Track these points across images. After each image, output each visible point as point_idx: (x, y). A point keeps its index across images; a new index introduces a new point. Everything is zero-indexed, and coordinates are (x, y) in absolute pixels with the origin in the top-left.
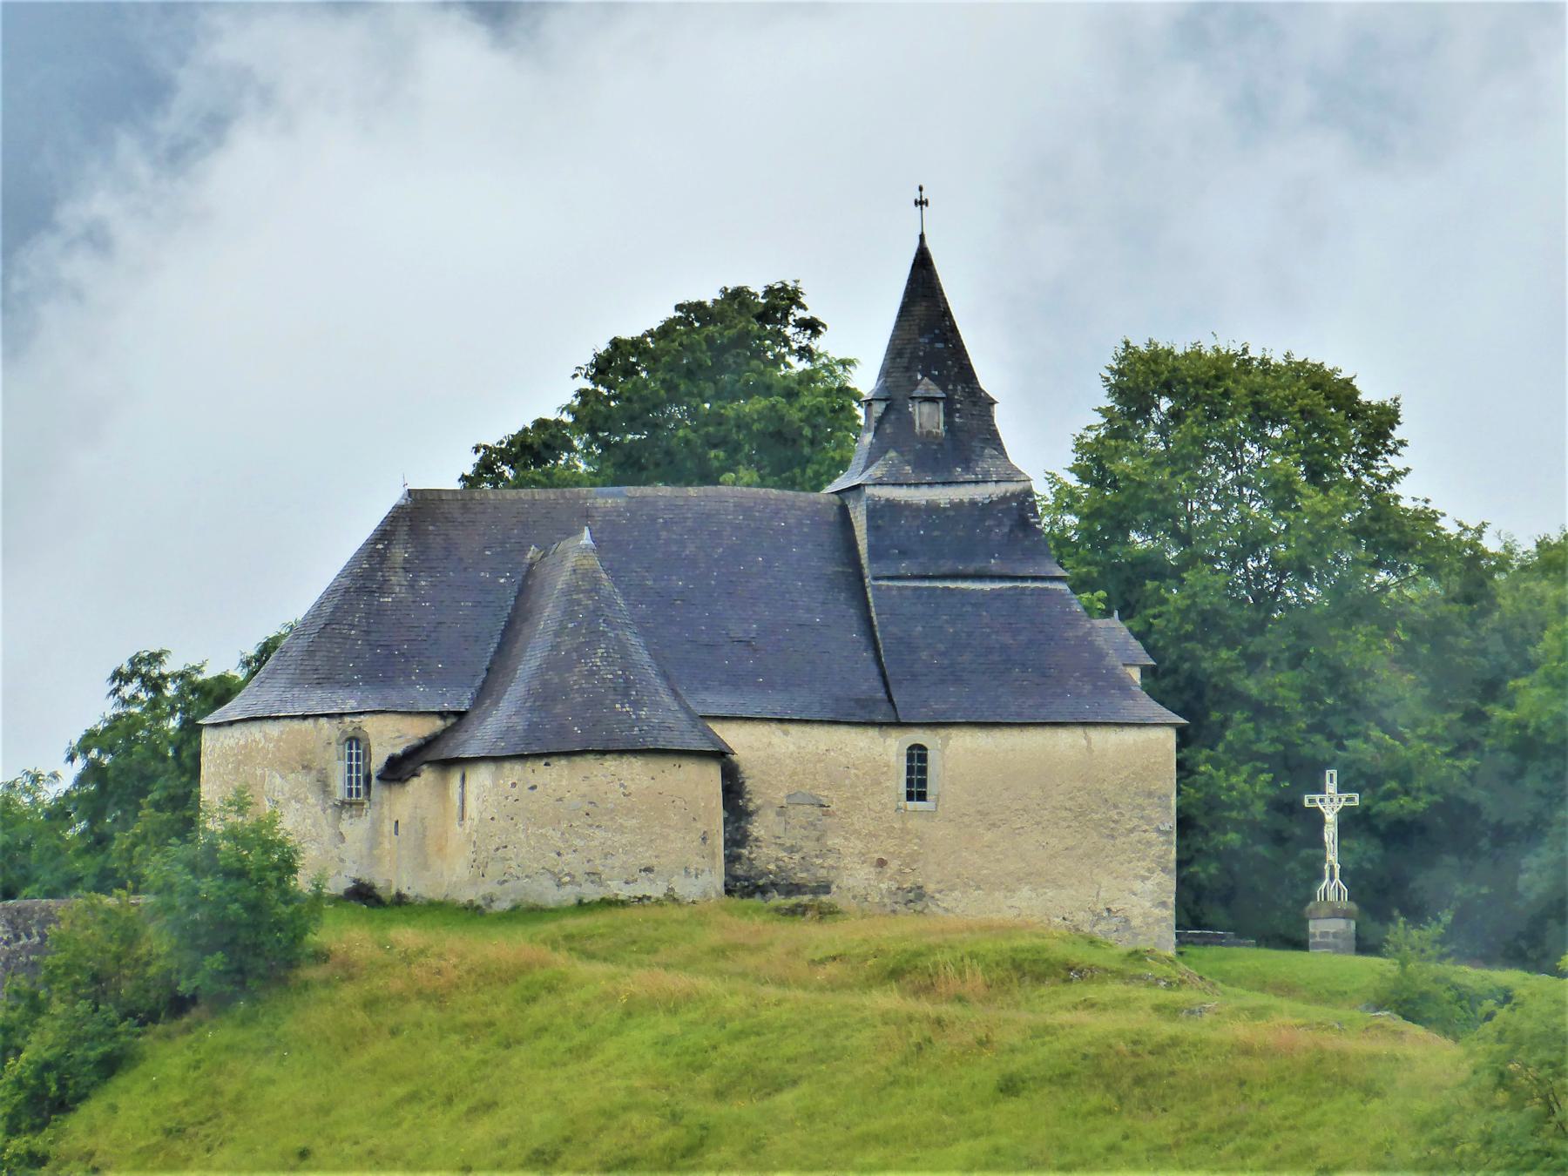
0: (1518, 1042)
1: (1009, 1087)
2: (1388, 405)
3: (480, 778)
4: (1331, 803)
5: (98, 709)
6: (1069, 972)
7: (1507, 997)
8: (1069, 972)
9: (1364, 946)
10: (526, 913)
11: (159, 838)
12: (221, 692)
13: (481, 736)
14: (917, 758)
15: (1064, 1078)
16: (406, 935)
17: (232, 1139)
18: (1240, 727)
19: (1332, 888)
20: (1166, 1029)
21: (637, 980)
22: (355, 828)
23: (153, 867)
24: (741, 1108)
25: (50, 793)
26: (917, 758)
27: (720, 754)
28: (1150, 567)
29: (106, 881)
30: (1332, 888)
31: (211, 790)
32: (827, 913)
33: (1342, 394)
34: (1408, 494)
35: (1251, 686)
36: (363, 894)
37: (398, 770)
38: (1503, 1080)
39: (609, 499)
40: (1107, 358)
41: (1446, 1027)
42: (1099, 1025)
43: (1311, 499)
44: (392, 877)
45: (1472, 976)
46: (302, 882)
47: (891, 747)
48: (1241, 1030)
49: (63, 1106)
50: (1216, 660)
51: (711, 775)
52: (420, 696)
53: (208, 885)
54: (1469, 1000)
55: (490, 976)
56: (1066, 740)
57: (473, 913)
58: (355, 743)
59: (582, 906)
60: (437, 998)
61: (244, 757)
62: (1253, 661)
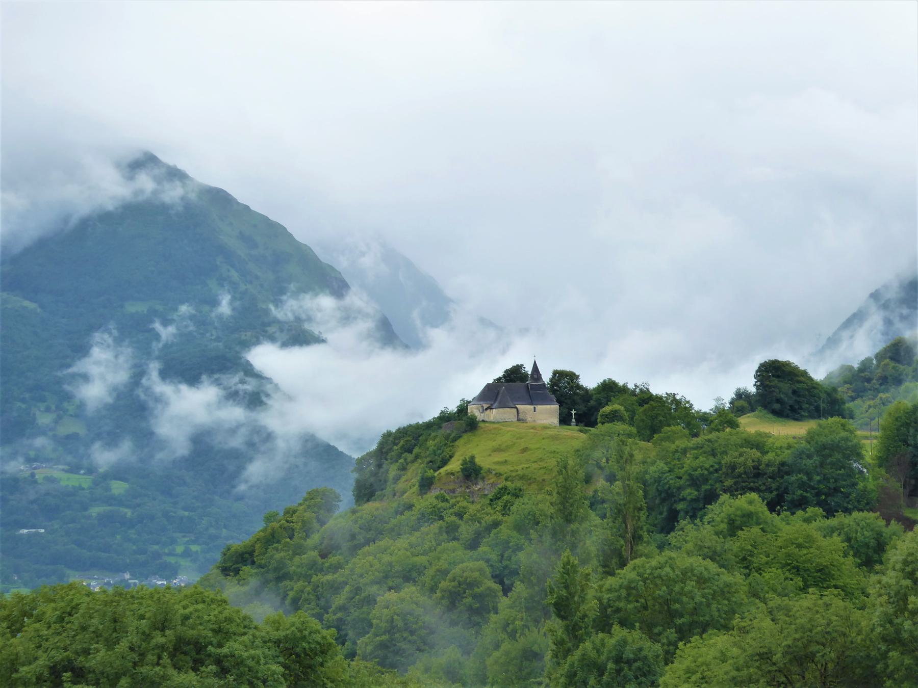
0: (591, 435)
1: (543, 439)
2: (482, 471)
3: (494, 410)
4: (573, 412)
5: (459, 404)
6: (549, 428)
7: (590, 430)
8: (549, 428)
9: (577, 425)
10: (498, 422)
11: (464, 416)
12: (470, 402)
13: (494, 406)
14: (535, 408)
15: (548, 438)
16: (487, 425)
17: (500, 433)
18: (564, 405)
19: (574, 420)
20: (558, 433)
21: (509, 429)
22: (482, 415)
23: (464, 418)
24: (518, 441)
25: (454, 411)
26: (535, 408)
27: (516, 408)
28: (556, 390)
29: (459, 420)
30: (574, 420)
31: (469, 411)
32: (526, 423)
33: (574, 374)
34: (580, 383)
35: (566, 401)
36: (483, 421)
37: (486, 409)
38: (590, 438)
39: (506, 384)
40: (552, 371)
41: (585, 433)
42: (552, 433)
43: (571, 384)
44: (486, 419)
45: (587, 428)
46: (478, 420)
47: (532, 407)
48: (565, 433)
49: (456, 441)
50: (563, 399)
51: (516, 410)
52: (488, 402)
53: (469, 420)
54: (586, 430)
55: (495, 428)
56: (548, 406)
57: (494, 423)
58: (482, 407)
59: (503, 422)
60: (490, 431)
61: (472, 408)
62: (566, 399)
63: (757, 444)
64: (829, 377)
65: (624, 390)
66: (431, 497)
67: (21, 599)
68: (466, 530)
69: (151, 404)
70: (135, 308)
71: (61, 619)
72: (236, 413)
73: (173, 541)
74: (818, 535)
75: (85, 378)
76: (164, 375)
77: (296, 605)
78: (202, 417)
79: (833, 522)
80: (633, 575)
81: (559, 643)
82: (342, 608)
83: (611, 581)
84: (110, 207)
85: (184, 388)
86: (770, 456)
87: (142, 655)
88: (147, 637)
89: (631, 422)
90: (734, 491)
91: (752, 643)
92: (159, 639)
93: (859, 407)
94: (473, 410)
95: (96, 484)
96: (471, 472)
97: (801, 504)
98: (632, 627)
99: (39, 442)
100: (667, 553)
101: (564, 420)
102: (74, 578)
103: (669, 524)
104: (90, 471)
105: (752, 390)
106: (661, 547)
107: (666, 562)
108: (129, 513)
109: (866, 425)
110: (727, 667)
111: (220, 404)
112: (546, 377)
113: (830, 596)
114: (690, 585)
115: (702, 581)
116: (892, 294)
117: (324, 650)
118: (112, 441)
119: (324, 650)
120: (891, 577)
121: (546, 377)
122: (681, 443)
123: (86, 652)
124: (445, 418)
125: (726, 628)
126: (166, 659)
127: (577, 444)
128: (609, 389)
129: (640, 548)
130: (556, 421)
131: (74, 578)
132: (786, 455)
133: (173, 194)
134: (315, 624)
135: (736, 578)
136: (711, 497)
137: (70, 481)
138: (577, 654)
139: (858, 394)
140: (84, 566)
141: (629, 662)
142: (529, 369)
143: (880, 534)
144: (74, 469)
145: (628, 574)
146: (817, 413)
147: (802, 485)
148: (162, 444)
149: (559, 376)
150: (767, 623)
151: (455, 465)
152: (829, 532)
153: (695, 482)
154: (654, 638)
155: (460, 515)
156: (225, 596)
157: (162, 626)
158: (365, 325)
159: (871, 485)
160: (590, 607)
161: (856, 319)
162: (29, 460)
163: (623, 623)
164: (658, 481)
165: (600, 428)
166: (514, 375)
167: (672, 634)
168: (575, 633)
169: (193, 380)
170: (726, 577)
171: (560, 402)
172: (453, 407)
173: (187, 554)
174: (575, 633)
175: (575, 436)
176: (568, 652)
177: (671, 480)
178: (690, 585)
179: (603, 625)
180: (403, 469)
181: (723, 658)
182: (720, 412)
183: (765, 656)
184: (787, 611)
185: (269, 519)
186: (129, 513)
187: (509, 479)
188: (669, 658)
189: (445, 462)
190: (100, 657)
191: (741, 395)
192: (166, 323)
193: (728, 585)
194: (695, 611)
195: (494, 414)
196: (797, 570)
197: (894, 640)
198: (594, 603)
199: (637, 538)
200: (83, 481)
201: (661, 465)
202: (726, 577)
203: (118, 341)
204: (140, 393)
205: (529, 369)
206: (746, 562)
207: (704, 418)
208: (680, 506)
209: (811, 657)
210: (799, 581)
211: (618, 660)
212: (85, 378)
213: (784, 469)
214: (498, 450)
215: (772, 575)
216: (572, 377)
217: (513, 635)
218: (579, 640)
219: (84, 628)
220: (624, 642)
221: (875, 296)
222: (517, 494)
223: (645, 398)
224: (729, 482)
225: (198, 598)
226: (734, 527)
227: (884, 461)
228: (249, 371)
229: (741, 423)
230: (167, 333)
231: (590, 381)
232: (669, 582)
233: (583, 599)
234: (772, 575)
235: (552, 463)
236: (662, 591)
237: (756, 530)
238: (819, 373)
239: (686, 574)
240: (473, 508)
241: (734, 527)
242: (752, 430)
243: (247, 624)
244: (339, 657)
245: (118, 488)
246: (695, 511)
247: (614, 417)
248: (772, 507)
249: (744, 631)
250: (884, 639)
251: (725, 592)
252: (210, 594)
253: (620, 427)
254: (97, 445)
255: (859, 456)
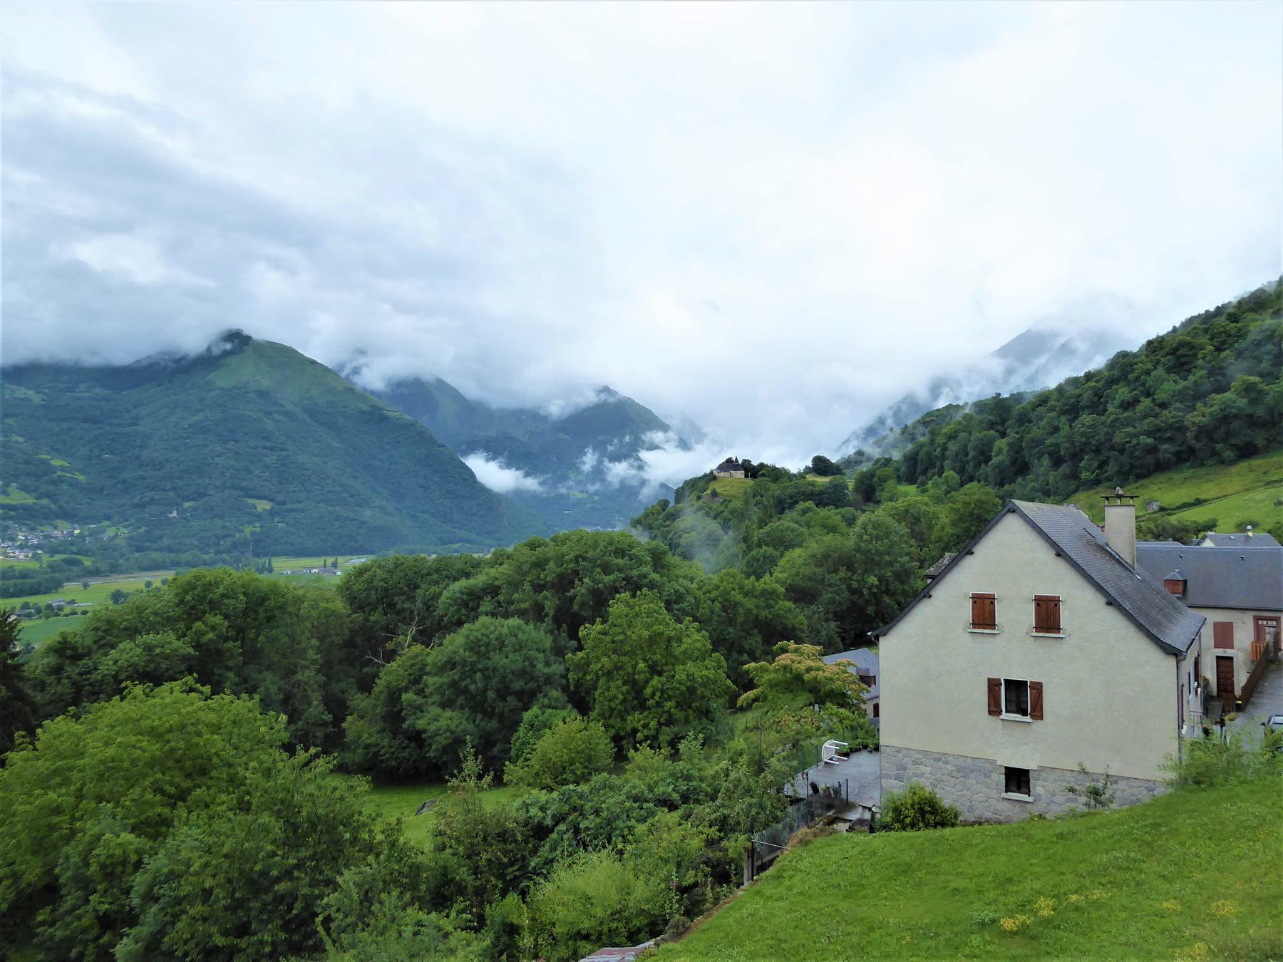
63: (813, 484)
64: (838, 461)
65: (767, 466)
66: (700, 502)
67: (565, 534)
68: (712, 514)
69: (605, 470)
70: (600, 438)
71: (578, 541)
72: (634, 472)
73: (615, 516)
74: (833, 516)
75: (584, 463)
76: (610, 461)
77: (654, 538)
78: (622, 473)
79: (838, 511)
80: (769, 529)
81: (744, 551)
82: (671, 539)
83: (762, 531)
84: (591, 405)
85: (617, 464)
86: (817, 488)
87: (605, 553)
88: (606, 547)
89: (769, 477)
90: (805, 500)
91: (810, 552)
92: (610, 548)
93: (846, 471)
94: (715, 473)
95: (589, 496)
96: (714, 494)
97: (827, 505)
98: (769, 546)
99: (571, 483)
100: (781, 521)
101: (746, 476)
102: (582, 528)
103: (782, 512)
104: (587, 492)
105: (811, 466)
106: (779, 519)
107: (559, 819)
108: (599, 506)
109: (849, 478)
110: (801, 559)
111: (628, 469)
112: (740, 462)
113: (837, 536)
114: (789, 532)
115: (793, 530)
116: (860, 432)
117: (665, 553)
118: (593, 483)
119: (665, 553)
120: (857, 529)
121: (740, 462)
122: (786, 484)
123: (586, 552)
124: (705, 475)
125: (802, 546)
126: (612, 555)
127: (751, 484)
128: (762, 466)
129: (772, 519)
130: (743, 476)
131: (582, 528)
132: (822, 488)
133: (612, 400)
134: (662, 544)
135: (804, 530)
136: (796, 502)
137: (580, 496)
138: (750, 555)
139: (847, 468)
140: (474, 553)
141: (768, 558)
142: (734, 459)
143: (854, 514)
144: (582, 492)
145: (767, 528)
146: (833, 474)
147: (828, 499)
148: (610, 483)
149: (745, 461)
150: (815, 545)
151: (709, 492)
152: (837, 514)
153: (791, 497)
154: (777, 550)
155: (710, 509)
156: (632, 534)
157: (611, 544)
158: (674, 444)
159: (851, 498)
160: (755, 539)
161: (846, 442)
162: (567, 489)
163: (766, 545)
164: (778, 497)
165: (759, 479)
166: (729, 461)
167: (782, 549)
168: (749, 548)
169: (620, 461)
170: (801, 529)
171: (745, 470)
172: (708, 472)
173: (619, 520)
174: (749, 548)
175: (750, 482)
176: (747, 554)
177: (783, 496)
178: (789, 532)
179: (759, 545)
180: (691, 492)
181: (800, 556)
182: (800, 473)
183: (814, 556)
184: (822, 541)
185: (646, 509)
186: (599, 506)
187: (1002, 430)
188: (781, 556)
189: (705, 491)
190: (591, 554)
191: (807, 468)
192: (611, 445)
193: (802, 532)
194: (790, 541)
195: (722, 474)
196: (825, 527)
197: (858, 550)
198: (756, 538)
199: (771, 516)
200: (584, 496)
201: (779, 492)
202: (801, 529)
203: (594, 451)
204: (602, 467)
205: (734, 459)
206: (808, 525)
207: (794, 475)
208: (786, 505)
209: (830, 556)
210: (826, 531)
211: (764, 557)
212: (584, 463)
213: (822, 493)
214: (722, 487)
215: (817, 529)
216: (749, 461)
217: (728, 549)
218: (750, 551)
219: (585, 544)
220: (766, 551)
221: (854, 433)
222: (730, 501)
223: (774, 469)
224: (802, 498)
225: (622, 534)
226: (804, 512)
227: (856, 490)
228: (638, 459)
229: (1018, 386)
230: (610, 448)
231: (755, 463)
232: (782, 531)
233: (752, 537)
234: (817, 529)
235: (742, 491)
236: (780, 534)
237: (811, 513)
238: (834, 460)
239: (788, 528)
240: (715, 506)
241: (804, 512)
242: (810, 479)
243: (639, 544)
244: (670, 555)
245: (596, 498)
246: (791, 507)
247: (764, 475)
248: (817, 506)
249: (807, 547)
250: (855, 550)
251: (801, 534)
252: (627, 533)
253: (766, 479)
254: (589, 485)
255: (847, 489)
